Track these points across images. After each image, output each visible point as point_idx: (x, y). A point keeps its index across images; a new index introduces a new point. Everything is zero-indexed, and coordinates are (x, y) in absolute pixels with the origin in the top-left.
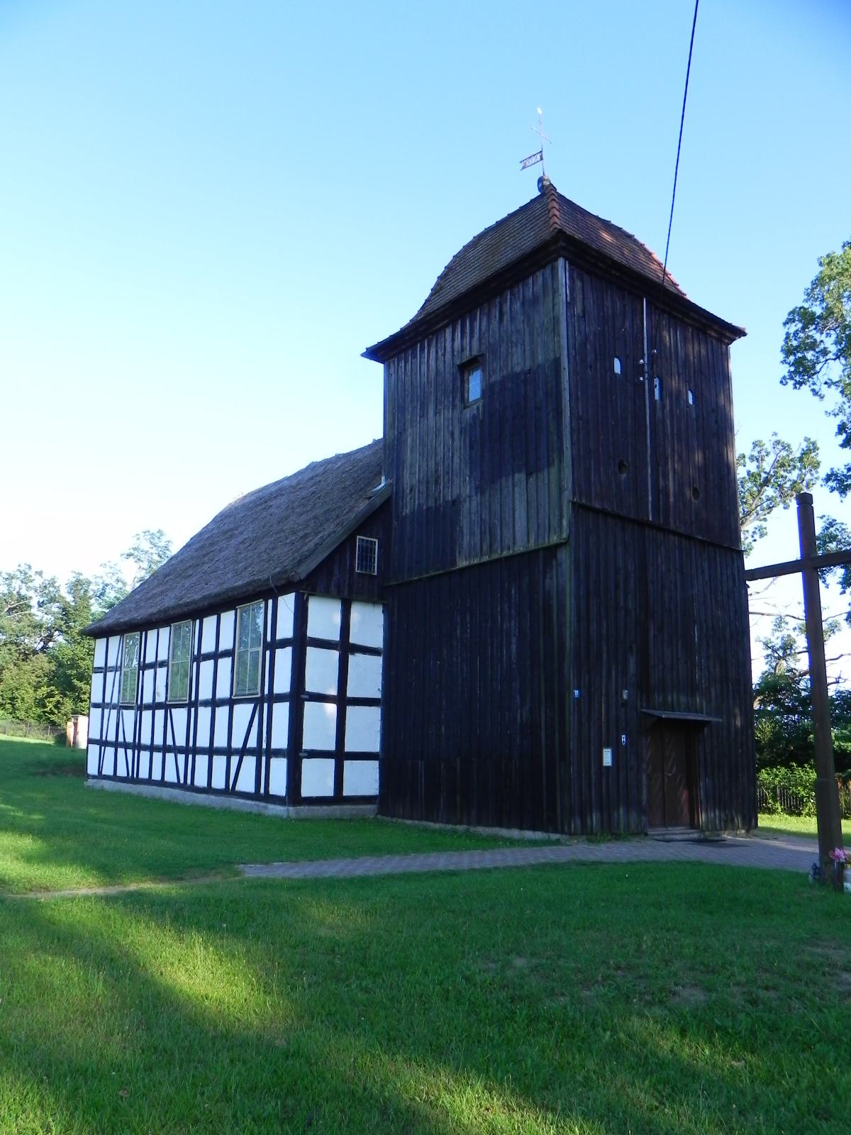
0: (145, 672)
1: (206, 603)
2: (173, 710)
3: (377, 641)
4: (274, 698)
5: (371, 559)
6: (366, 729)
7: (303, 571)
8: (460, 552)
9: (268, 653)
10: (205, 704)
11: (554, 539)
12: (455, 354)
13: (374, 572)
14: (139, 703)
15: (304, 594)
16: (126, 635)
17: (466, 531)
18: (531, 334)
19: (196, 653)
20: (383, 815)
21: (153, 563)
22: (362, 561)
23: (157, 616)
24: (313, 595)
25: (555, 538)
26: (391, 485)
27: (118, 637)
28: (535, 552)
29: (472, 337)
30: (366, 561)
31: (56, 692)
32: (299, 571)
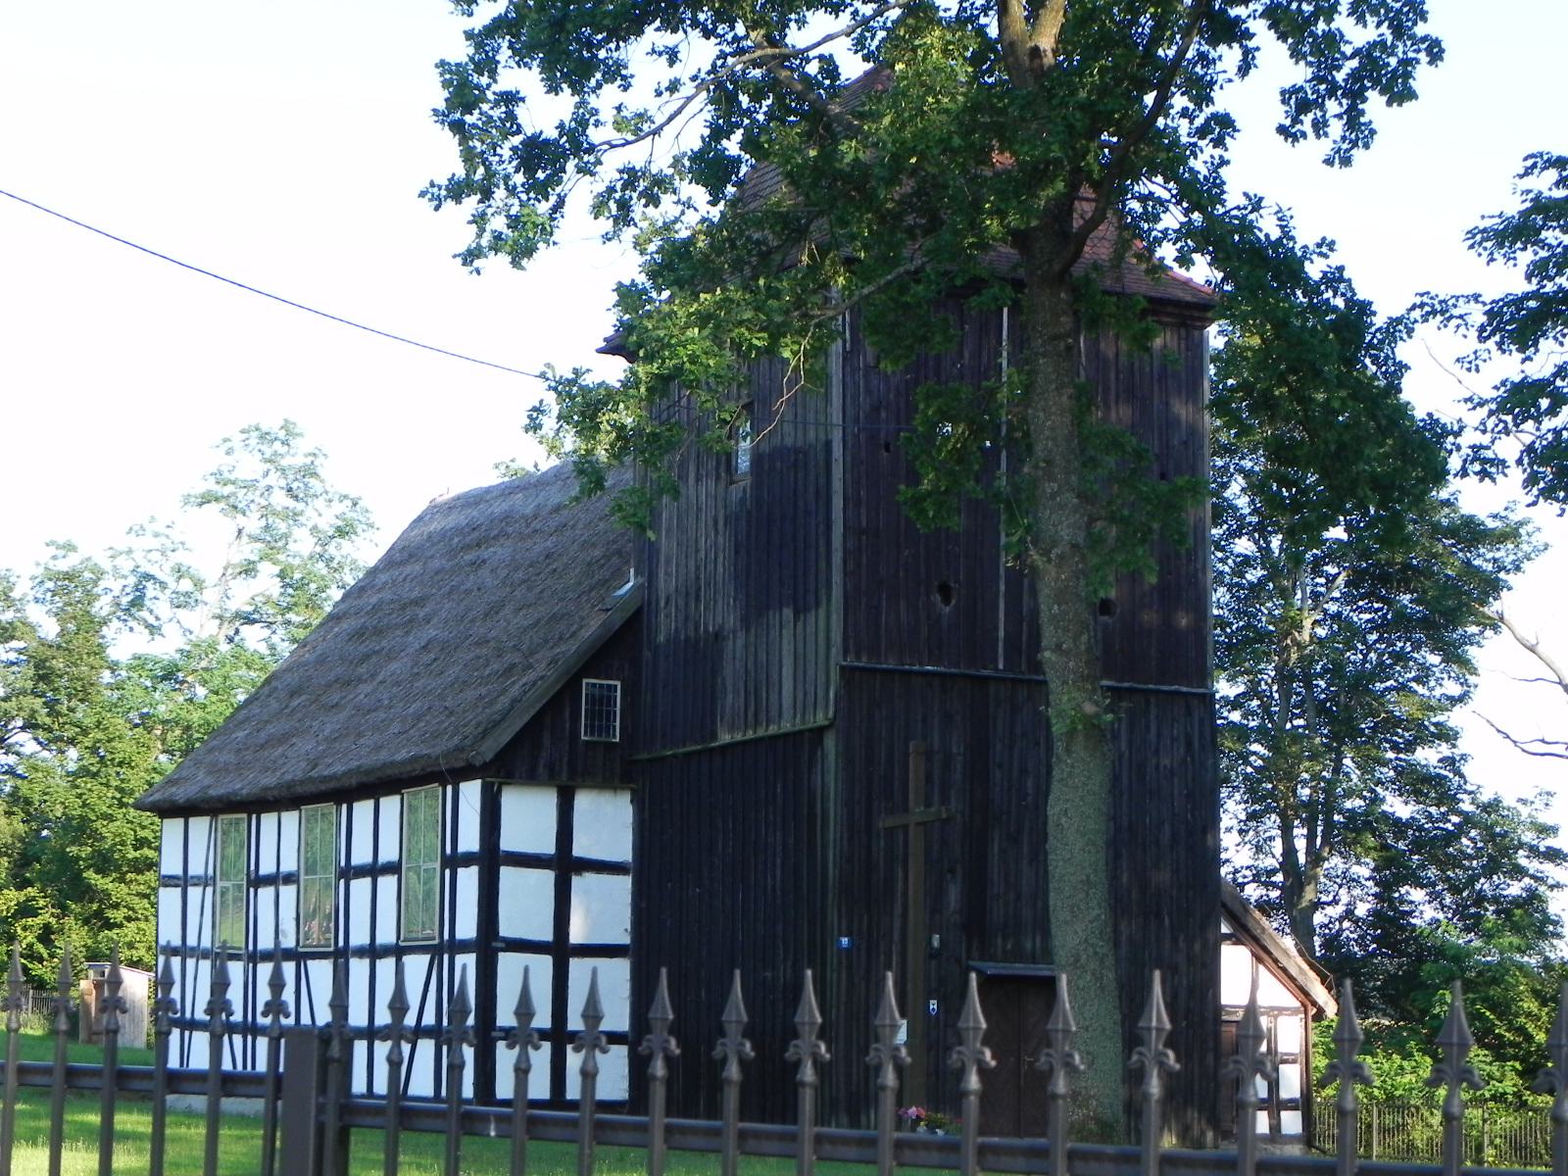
0: (260, 890)
1: (354, 782)
2: (309, 962)
3: (622, 850)
4: (457, 947)
5: (610, 716)
7: (489, 749)
9: (447, 872)
10: (361, 952)
13: (614, 736)
14: (251, 948)
15: (493, 784)
16: (221, 817)
17: (730, 688)
19: (343, 864)
21: (275, 514)
22: (593, 720)
23: (276, 793)
24: (509, 784)
26: (643, 585)
27: (207, 819)
30: (600, 720)
31: (42, 903)
32: (483, 749)
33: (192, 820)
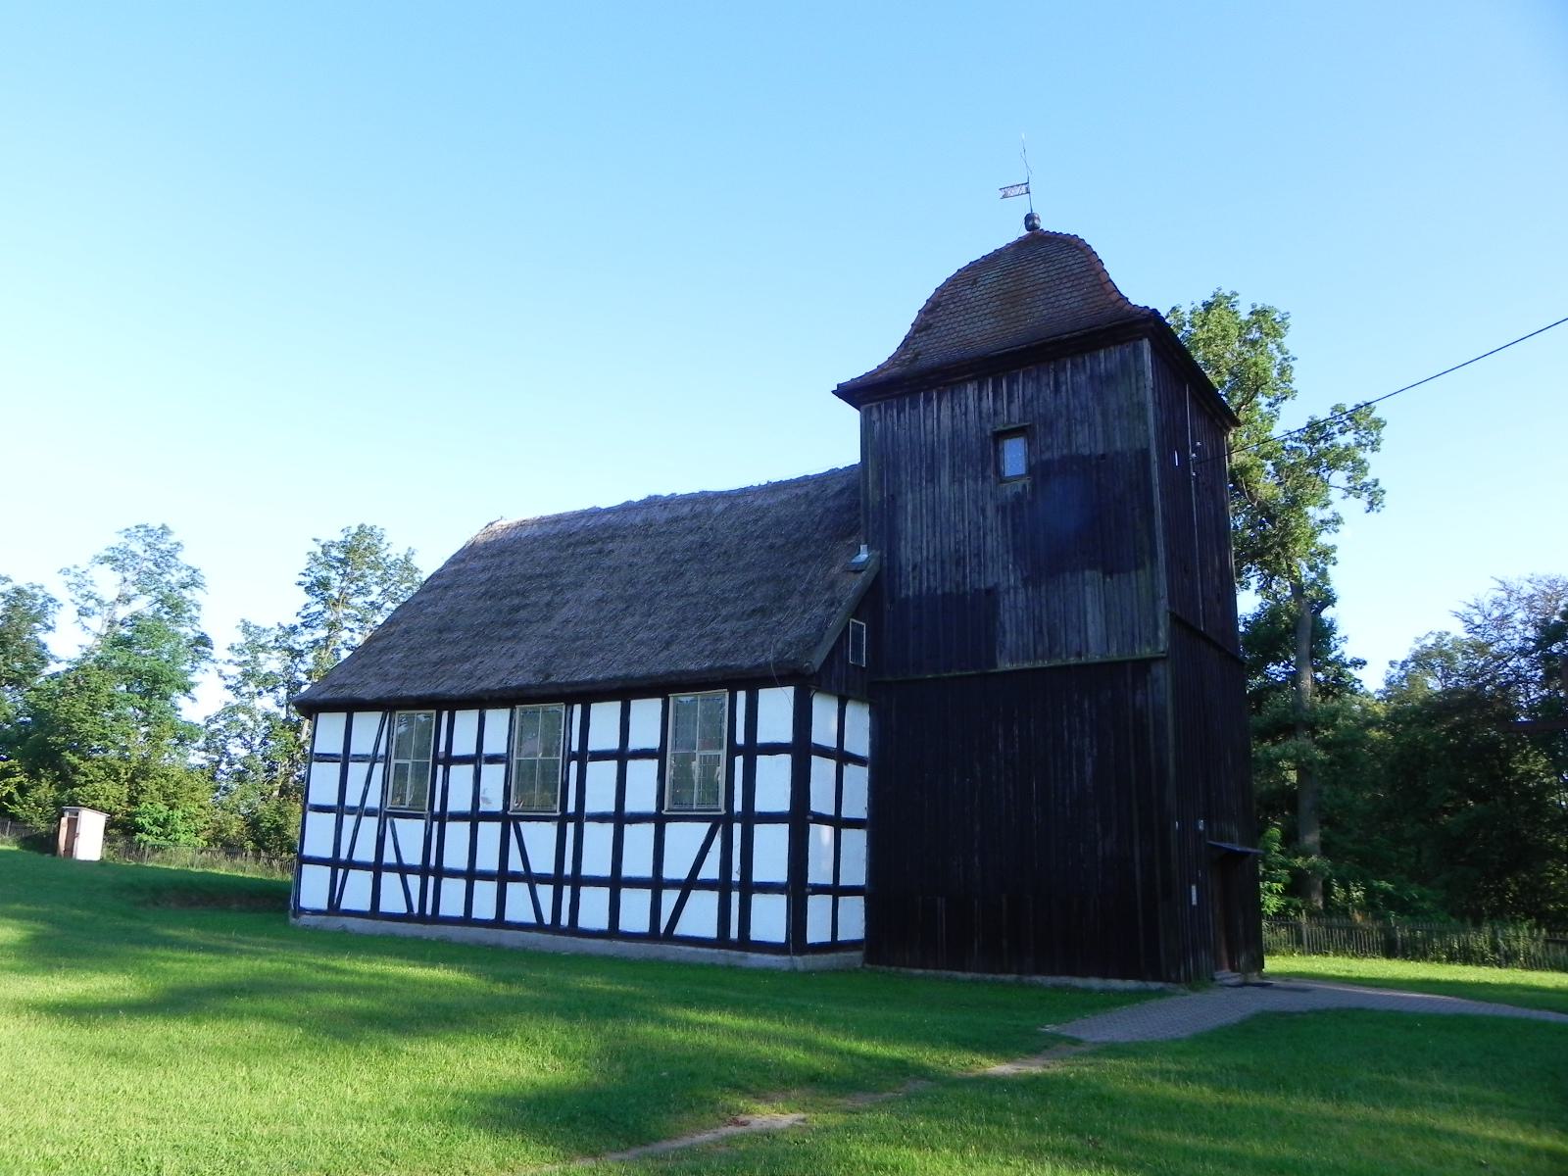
6: (842, 856)
8: (1001, 652)
11: (1147, 652)
12: (984, 415)
18: (1104, 415)
20: (872, 964)
25: (1148, 650)
28: (1119, 665)
29: (1010, 402)
33: (357, 716)
